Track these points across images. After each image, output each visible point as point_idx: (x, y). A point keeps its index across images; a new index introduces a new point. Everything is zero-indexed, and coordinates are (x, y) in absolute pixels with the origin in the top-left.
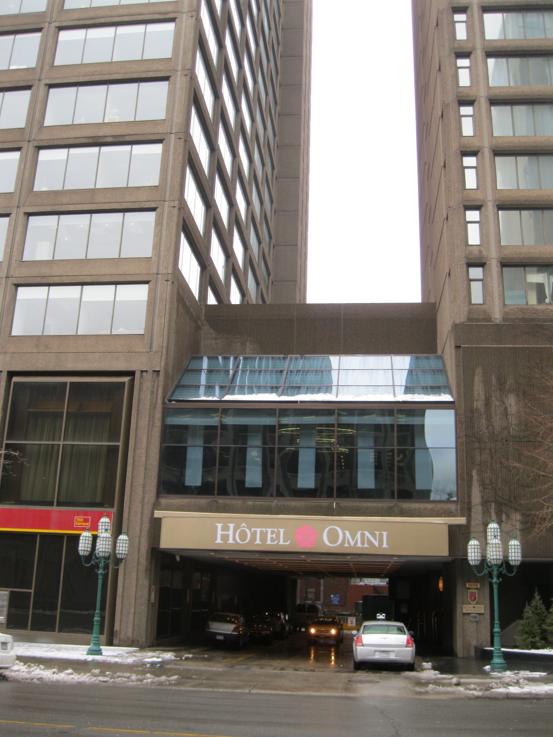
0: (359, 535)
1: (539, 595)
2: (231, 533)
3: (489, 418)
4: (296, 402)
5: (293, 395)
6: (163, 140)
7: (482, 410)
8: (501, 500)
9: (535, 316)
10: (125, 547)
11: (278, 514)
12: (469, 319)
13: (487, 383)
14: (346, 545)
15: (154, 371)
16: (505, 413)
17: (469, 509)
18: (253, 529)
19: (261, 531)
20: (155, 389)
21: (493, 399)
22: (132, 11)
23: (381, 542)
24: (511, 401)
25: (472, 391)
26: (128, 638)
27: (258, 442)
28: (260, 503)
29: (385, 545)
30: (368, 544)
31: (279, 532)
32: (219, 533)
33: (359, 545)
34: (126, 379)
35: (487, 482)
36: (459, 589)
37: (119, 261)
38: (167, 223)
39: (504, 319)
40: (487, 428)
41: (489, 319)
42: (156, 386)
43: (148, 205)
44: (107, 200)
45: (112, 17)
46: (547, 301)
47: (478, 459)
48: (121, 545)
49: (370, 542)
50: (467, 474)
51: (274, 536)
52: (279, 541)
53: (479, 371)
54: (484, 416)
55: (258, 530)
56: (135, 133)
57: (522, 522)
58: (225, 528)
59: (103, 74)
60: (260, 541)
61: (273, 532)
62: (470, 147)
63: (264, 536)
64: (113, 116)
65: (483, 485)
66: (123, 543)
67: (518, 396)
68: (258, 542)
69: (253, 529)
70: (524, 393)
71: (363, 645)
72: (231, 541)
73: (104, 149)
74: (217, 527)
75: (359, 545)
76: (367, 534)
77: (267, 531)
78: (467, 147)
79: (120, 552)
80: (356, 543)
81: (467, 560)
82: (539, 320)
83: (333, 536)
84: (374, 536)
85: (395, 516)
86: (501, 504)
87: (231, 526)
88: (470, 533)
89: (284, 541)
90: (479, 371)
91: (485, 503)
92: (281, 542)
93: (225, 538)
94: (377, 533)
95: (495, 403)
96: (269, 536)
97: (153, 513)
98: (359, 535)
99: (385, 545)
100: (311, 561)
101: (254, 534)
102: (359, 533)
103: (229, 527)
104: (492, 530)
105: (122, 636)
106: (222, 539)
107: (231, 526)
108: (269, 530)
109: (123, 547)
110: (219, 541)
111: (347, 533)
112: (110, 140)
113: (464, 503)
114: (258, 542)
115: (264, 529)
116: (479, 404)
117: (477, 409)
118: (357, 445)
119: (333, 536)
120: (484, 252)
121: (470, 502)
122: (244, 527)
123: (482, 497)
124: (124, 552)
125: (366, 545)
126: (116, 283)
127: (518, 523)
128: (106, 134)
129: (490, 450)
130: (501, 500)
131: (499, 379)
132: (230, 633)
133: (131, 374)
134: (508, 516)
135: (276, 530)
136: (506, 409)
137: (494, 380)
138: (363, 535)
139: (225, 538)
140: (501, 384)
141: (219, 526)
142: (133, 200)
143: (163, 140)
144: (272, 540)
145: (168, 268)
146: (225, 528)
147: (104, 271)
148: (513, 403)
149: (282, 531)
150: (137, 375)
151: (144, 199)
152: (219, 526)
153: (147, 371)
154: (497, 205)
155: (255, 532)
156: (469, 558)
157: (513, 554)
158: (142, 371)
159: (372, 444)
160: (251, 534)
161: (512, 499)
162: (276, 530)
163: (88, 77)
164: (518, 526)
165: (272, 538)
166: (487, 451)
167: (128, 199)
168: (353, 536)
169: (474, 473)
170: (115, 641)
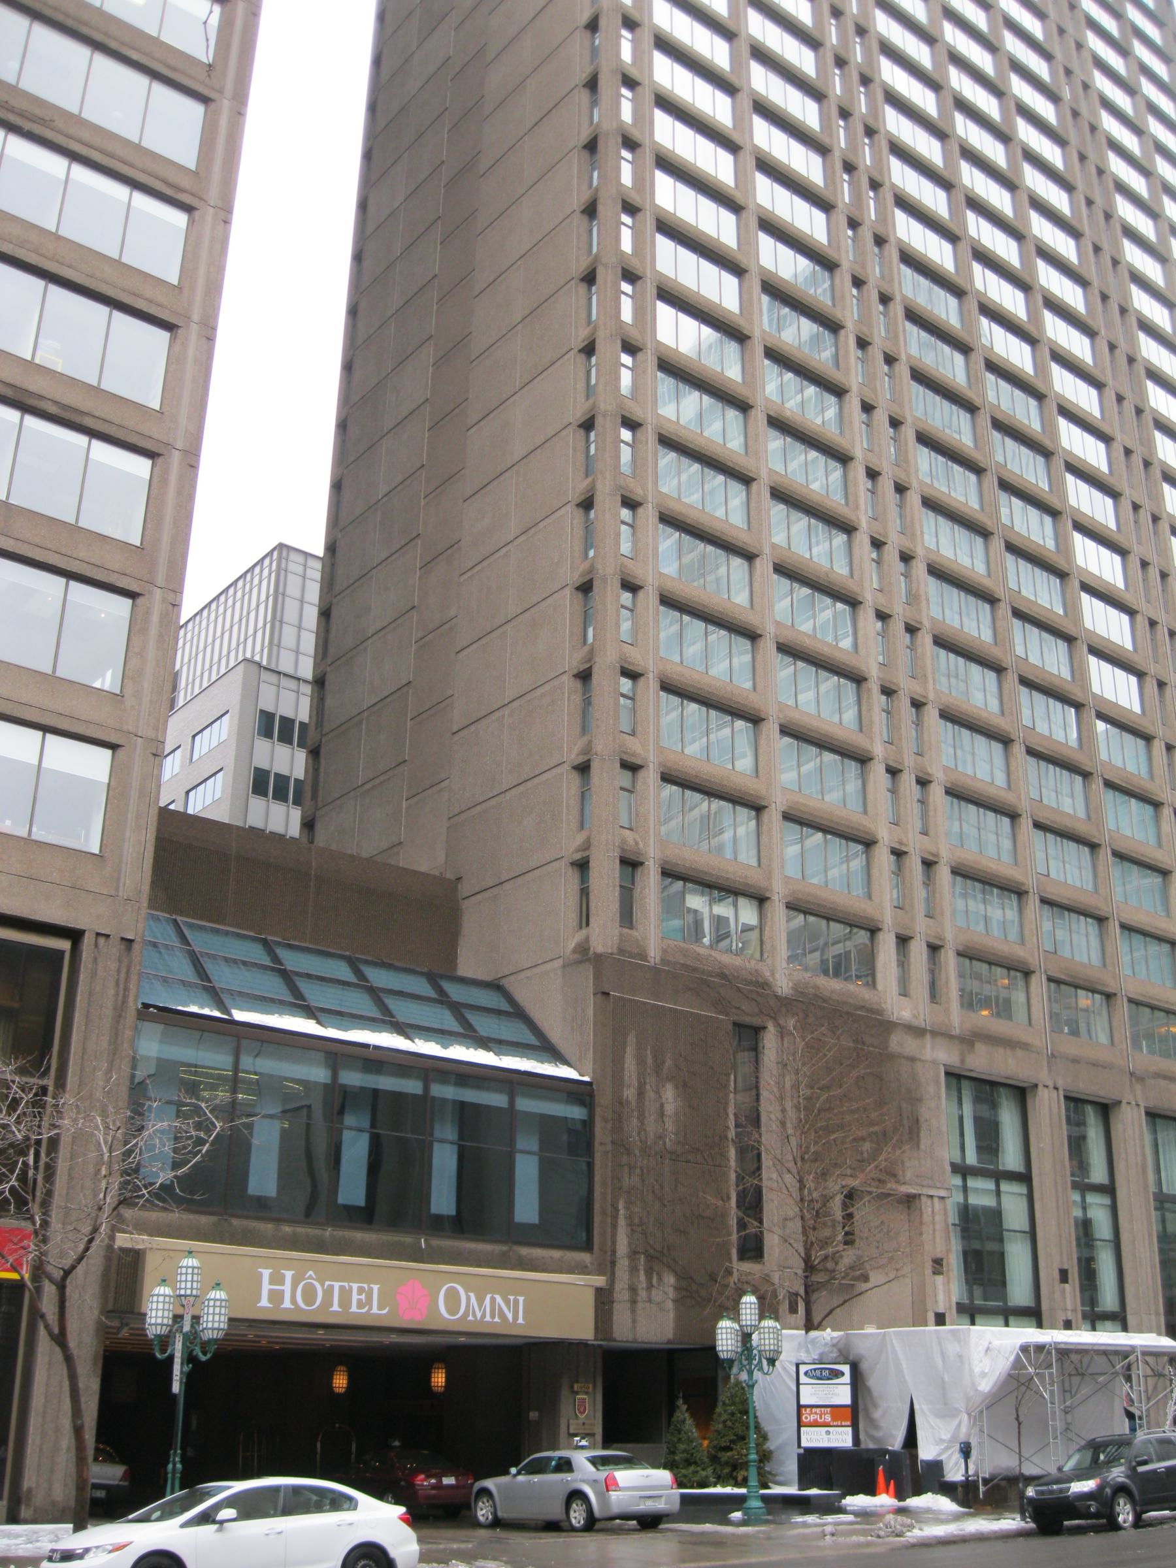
0: (487, 1301)
1: (684, 1403)
2: (287, 1288)
3: (642, 1118)
4: (366, 1046)
5: (345, 1029)
6: (159, 455)
7: (634, 1104)
8: (652, 1251)
9: (697, 964)
10: (220, 1314)
11: (338, 1255)
12: (621, 951)
13: (640, 1060)
14: (471, 1318)
15: (123, 939)
16: (661, 1114)
17: (613, 1263)
18: (327, 1283)
19: (342, 1288)
20: (123, 976)
21: (648, 1087)
22: (111, 147)
23: (516, 1316)
24: (669, 1094)
25: (623, 1069)
26: (54, 1503)
27: (533, 1144)
28: (303, 1230)
29: (520, 1321)
30: (500, 1317)
31: (371, 1290)
32: (266, 1287)
33: (488, 1318)
34: (65, 945)
35: (637, 1221)
36: (565, 1393)
37: (51, 681)
38: (161, 635)
39: (664, 961)
40: (639, 1133)
41: (644, 957)
42: (124, 970)
43: (123, 583)
44: (36, 540)
45: (67, 136)
46: (706, 941)
47: (626, 1182)
48: (724, 1336)
49: (502, 1315)
50: (612, 1206)
51: (363, 1297)
52: (371, 1308)
53: (631, 1039)
54: (636, 1114)
55: (337, 1285)
56: (103, 416)
57: (676, 1289)
58: (277, 1279)
59: (42, 255)
60: (340, 1306)
61: (361, 1291)
62: (633, 664)
63: (345, 1295)
64: (51, 356)
65: (631, 1224)
66: (214, 1306)
67: (677, 1087)
68: (336, 1307)
69: (327, 1283)
70: (685, 1085)
71: (620, 1489)
72: (287, 1304)
73: (31, 421)
74: (261, 1275)
75: (488, 1318)
76: (499, 1299)
77: (351, 1288)
78: (629, 663)
79: (210, 1325)
80: (484, 1315)
81: (712, 1349)
82: (703, 972)
83: (453, 1300)
84: (507, 1302)
85: (512, 1269)
86: (652, 1257)
87: (289, 1275)
88: (613, 1302)
89: (380, 1308)
90: (631, 1039)
91: (633, 1255)
92: (375, 1310)
93: (276, 1297)
94: (512, 1298)
95: (650, 1095)
96: (355, 1297)
97: (112, 1238)
98: (487, 1301)
99: (520, 1321)
100: (256, 1336)
101: (328, 1293)
102: (489, 1296)
103: (283, 1276)
104: (190, 1271)
105: (39, 1499)
106: (270, 1300)
107: (289, 1275)
108: (355, 1286)
109: (214, 1314)
110: (264, 1302)
111: (472, 1295)
112: (52, 409)
113: (606, 1252)
114: (336, 1307)
115: (346, 1284)
116: (630, 1093)
117: (628, 1102)
118: (432, 1134)
119: (453, 1300)
120: (641, 846)
121: (614, 1252)
122: (310, 1277)
123: (630, 1244)
124: (216, 1325)
125: (496, 1319)
126: (46, 729)
127: (671, 1289)
128: (44, 393)
129: (642, 1170)
130: (652, 1251)
131: (655, 1057)
132: (116, 1483)
133: (75, 935)
134: (660, 1279)
135: (365, 1286)
136: (662, 1106)
137: (650, 1060)
138: (493, 1300)
139: (276, 1297)
140: (658, 1067)
141: (266, 1273)
142: (93, 561)
143: (159, 455)
144: (360, 1304)
145: (157, 730)
146: (277, 1279)
147: (25, 696)
148: (671, 1100)
149: (376, 1288)
150: (88, 941)
151: (116, 567)
152: (266, 1273)
153: (108, 936)
154: (662, 773)
155: (332, 1287)
156: (719, 1348)
157: (724, 1342)
158: (98, 934)
159: (366, 1124)
160: (325, 1292)
161: (665, 1251)
162: (365, 1286)
163: (11, 246)
164: (671, 1292)
165: (359, 1301)
166: (638, 1171)
167: (82, 554)
168: (481, 1302)
169: (621, 1205)
170: (24, 1512)
